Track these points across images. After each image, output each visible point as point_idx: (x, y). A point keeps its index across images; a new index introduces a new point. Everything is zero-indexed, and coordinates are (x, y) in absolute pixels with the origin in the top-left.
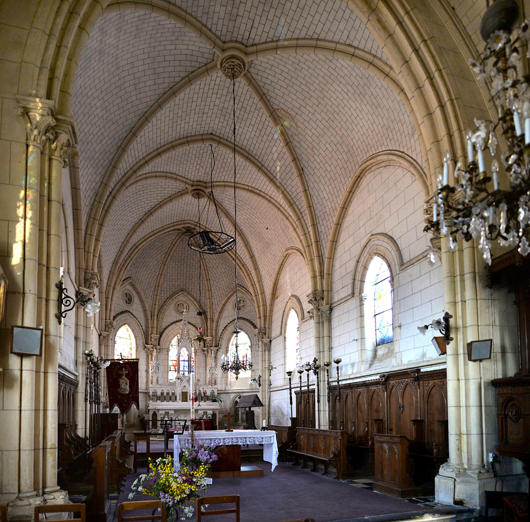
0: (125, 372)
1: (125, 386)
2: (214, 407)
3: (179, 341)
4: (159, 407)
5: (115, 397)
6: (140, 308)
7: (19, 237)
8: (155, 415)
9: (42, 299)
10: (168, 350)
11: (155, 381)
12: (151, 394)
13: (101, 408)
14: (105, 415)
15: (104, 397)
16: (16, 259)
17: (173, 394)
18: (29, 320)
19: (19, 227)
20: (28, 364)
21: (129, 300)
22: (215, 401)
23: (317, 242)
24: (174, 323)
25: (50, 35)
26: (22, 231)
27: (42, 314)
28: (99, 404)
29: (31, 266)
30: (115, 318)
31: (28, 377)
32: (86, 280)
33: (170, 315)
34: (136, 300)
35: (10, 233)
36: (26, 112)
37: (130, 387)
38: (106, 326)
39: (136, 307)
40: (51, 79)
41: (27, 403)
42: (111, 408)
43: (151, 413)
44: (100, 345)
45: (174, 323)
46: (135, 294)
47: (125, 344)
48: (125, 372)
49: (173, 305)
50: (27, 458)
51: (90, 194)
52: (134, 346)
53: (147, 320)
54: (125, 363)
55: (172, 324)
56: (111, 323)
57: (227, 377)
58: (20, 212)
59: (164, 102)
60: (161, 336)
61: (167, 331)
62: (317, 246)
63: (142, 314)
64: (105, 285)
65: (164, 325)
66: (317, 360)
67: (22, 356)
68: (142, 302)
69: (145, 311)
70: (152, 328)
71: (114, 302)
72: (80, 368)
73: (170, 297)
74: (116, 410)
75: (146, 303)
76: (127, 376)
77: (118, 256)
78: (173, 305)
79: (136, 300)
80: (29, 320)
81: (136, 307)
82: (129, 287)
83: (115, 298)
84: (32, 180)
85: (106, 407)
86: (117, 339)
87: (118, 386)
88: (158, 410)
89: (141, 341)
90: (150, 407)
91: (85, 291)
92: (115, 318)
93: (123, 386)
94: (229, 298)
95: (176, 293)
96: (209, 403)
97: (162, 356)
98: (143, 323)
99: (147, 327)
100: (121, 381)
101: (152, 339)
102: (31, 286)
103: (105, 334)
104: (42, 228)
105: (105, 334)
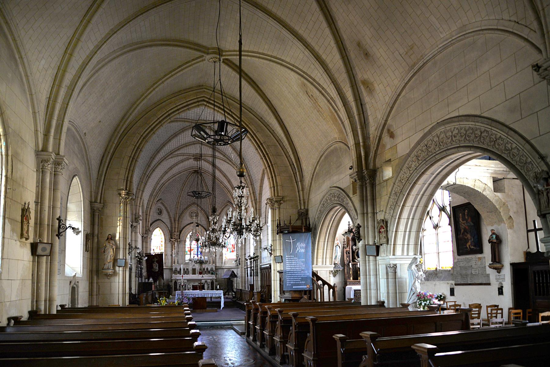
0: (156, 260)
1: (156, 267)
2: (211, 278)
3: (191, 236)
4: (178, 278)
5: (151, 273)
6: (167, 217)
7: (118, 231)
8: (176, 283)
9: (125, 249)
10: (185, 241)
11: (176, 261)
12: (174, 269)
13: (143, 279)
14: (145, 283)
15: (144, 273)
16: (117, 238)
17: (187, 269)
18: (121, 257)
19: (118, 228)
20: (121, 269)
21: (160, 213)
22: (212, 274)
23: (253, 193)
24: (189, 224)
25: (127, 169)
26: (119, 229)
27: (125, 254)
28: (142, 277)
29: (122, 239)
30: (151, 224)
31: (121, 273)
32: (136, 219)
33: (187, 219)
34: (165, 212)
35: (116, 230)
36: (120, 194)
37: (159, 268)
38: (146, 231)
39: (165, 217)
40: (127, 181)
41: (121, 280)
42: (148, 280)
43: (173, 282)
44: (143, 242)
45: (189, 224)
46: (164, 208)
47: (158, 242)
48: (156, 260)
49: (188, 213)
50: (121, 296)
51: (138, 179)
52: (164, 240)
53: (171, 223)
54: (155, 255)
55: (187, 225)
56: (149, 230)
57: (222, 259)
58: (118, 224)
59: (171, 139)
60: (180, 233)
61: (184, 230)
62: (254, 195)
63: (169, 220)
64: (145, 207)
65: (182, 227)
66: (361, 227)
67: (119, 267)
68: (168, 212)
69: (170, 218)
70: (175, 228)
71: (162, 85)
72: (133, 261)
73: (186, 208)
74: (151, 280)
75: (171, 213)
76: (157, 262)
77: (153, 192)
78: (188, 213)
79: (165, 212)
80: (121, 257)
81: (165, 217)
82: (160, 205)
83: (151, 213)
84: (122, 214)
85: (146, 279)
86: (153, 237)
87: (152, 267)
88: (178, 280)
89: (168, 237)
90: (173, 278)
91: (135, 224)
92: (151, 224)
93: (155, 267)
94: (223, 209)
95: (190, 205)
96: (210, 275)
97: (181, 246)
98: (169, 226)
99: (172, 228)
100: (154, 265)
101: (174, 237)
102: (121, 246)
103: (145, 235)
104: (125, 227)
105: (145, 235)
